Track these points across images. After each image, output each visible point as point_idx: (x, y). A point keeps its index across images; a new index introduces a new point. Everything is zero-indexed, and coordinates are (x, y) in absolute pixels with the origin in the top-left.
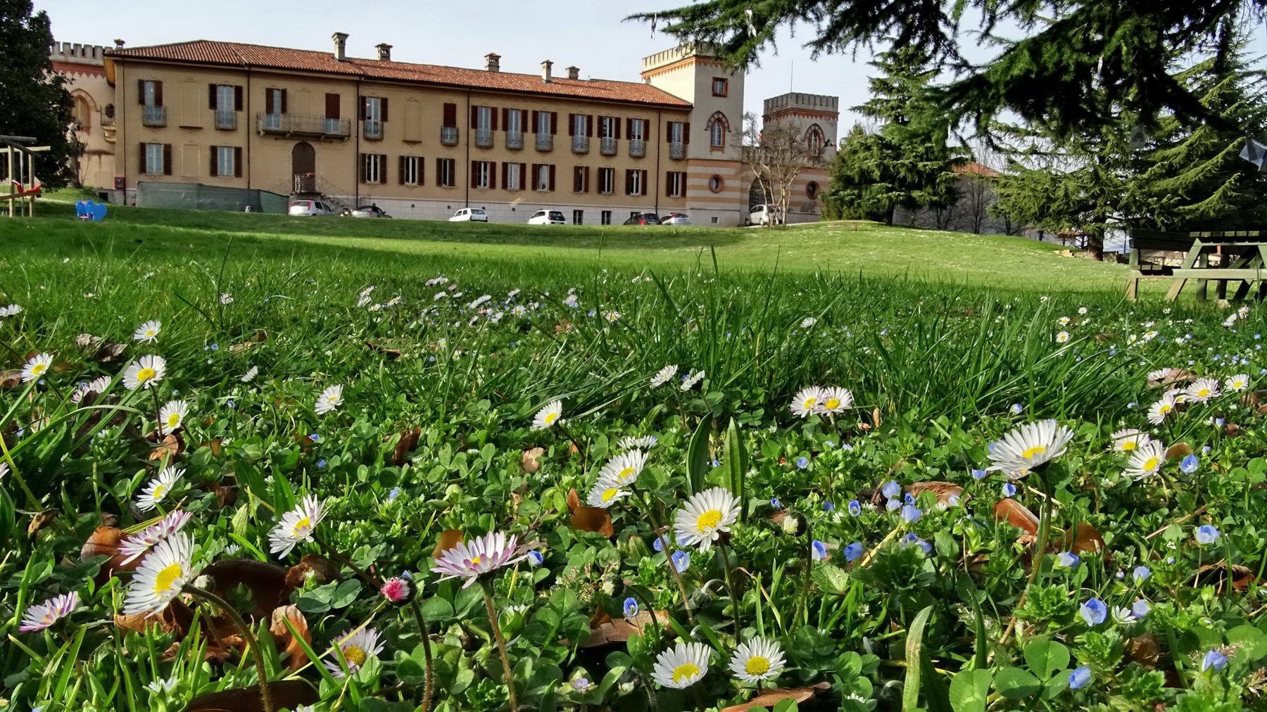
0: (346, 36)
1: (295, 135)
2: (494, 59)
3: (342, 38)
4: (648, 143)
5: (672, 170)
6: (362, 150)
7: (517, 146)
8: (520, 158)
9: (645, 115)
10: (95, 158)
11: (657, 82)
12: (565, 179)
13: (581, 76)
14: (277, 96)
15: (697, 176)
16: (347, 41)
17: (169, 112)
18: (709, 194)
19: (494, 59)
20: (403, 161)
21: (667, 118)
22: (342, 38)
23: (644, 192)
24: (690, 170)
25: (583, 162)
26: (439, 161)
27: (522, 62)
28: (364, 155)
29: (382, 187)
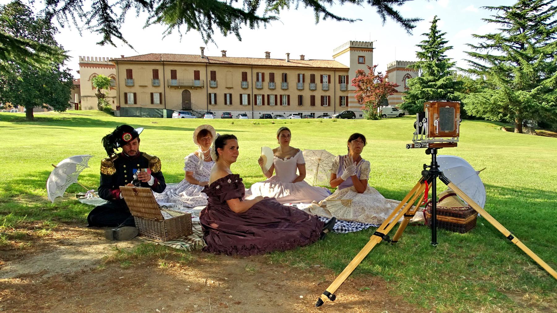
1: (182, 87)
2: (268, 54)
4: (305, 84)
7: (327, 89)
9: (328, 73)
10: (85, 98)
13: (306, 58)
14: (260, 75)
17: (135, 81)
19: (268, 54)
20: (322, 97)
24: (349, 95)
26: (322, 96)
28: (210, 94)
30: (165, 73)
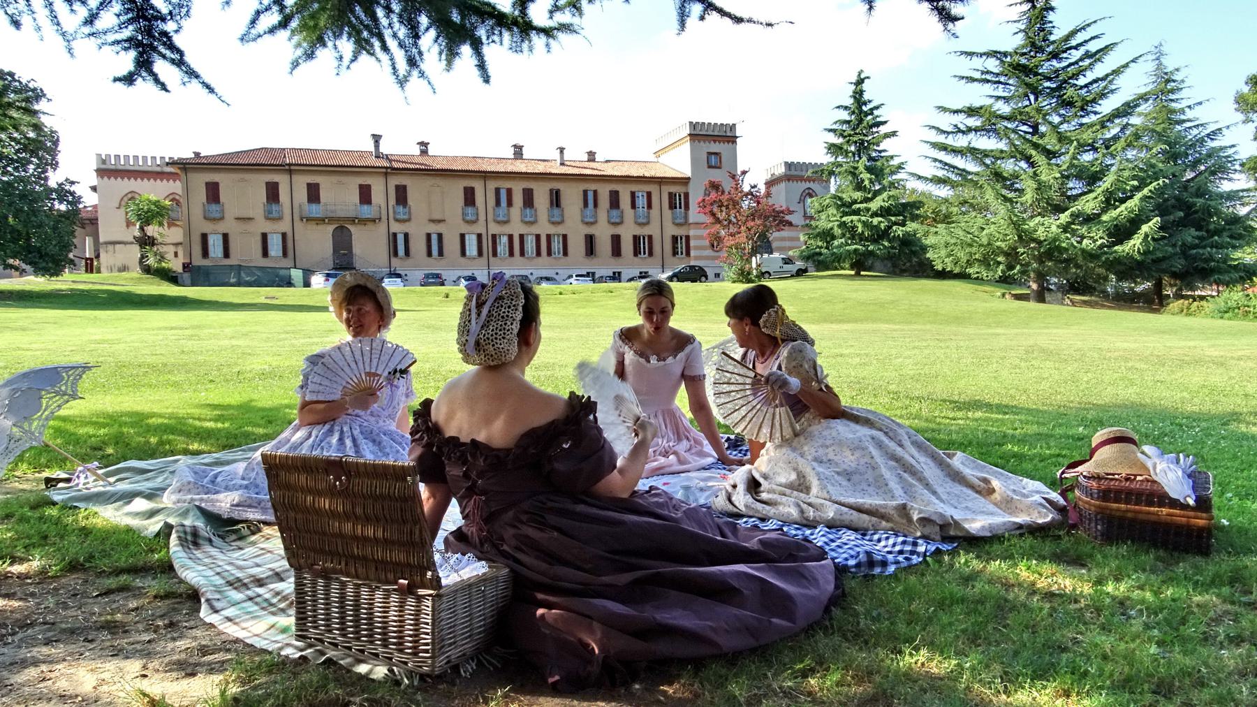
0: (380, 137)
1: (331, 220)
3: (377, 139)
5: (637, 233)
6: (392, 230)
14: (590, 195)
15: (700, 238)
16: (381, 142)
17: (226, 207)
18: (709, 252)
19: (518, 151)
20: (636, 239)
21: (492, 185)
22: (377, 139)
23: (651, 254)
24: (692, 233)
25: (617, 231)
28: (395, 235)
30: (294, 191)
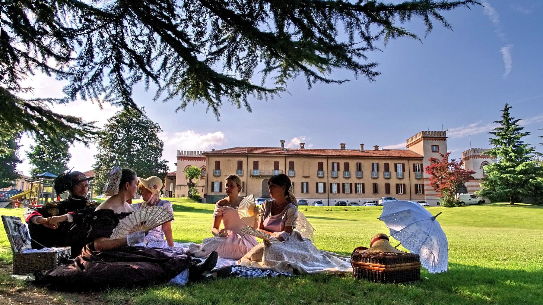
5: (398, 183)
8: (349, 181)
9: (403, 162)
10: (179, 187)
11: (410, 149)
12: (369, 189)
23: (405, 193)
24: (425, 183)
27: (353, 146)
29: (404, 195)
